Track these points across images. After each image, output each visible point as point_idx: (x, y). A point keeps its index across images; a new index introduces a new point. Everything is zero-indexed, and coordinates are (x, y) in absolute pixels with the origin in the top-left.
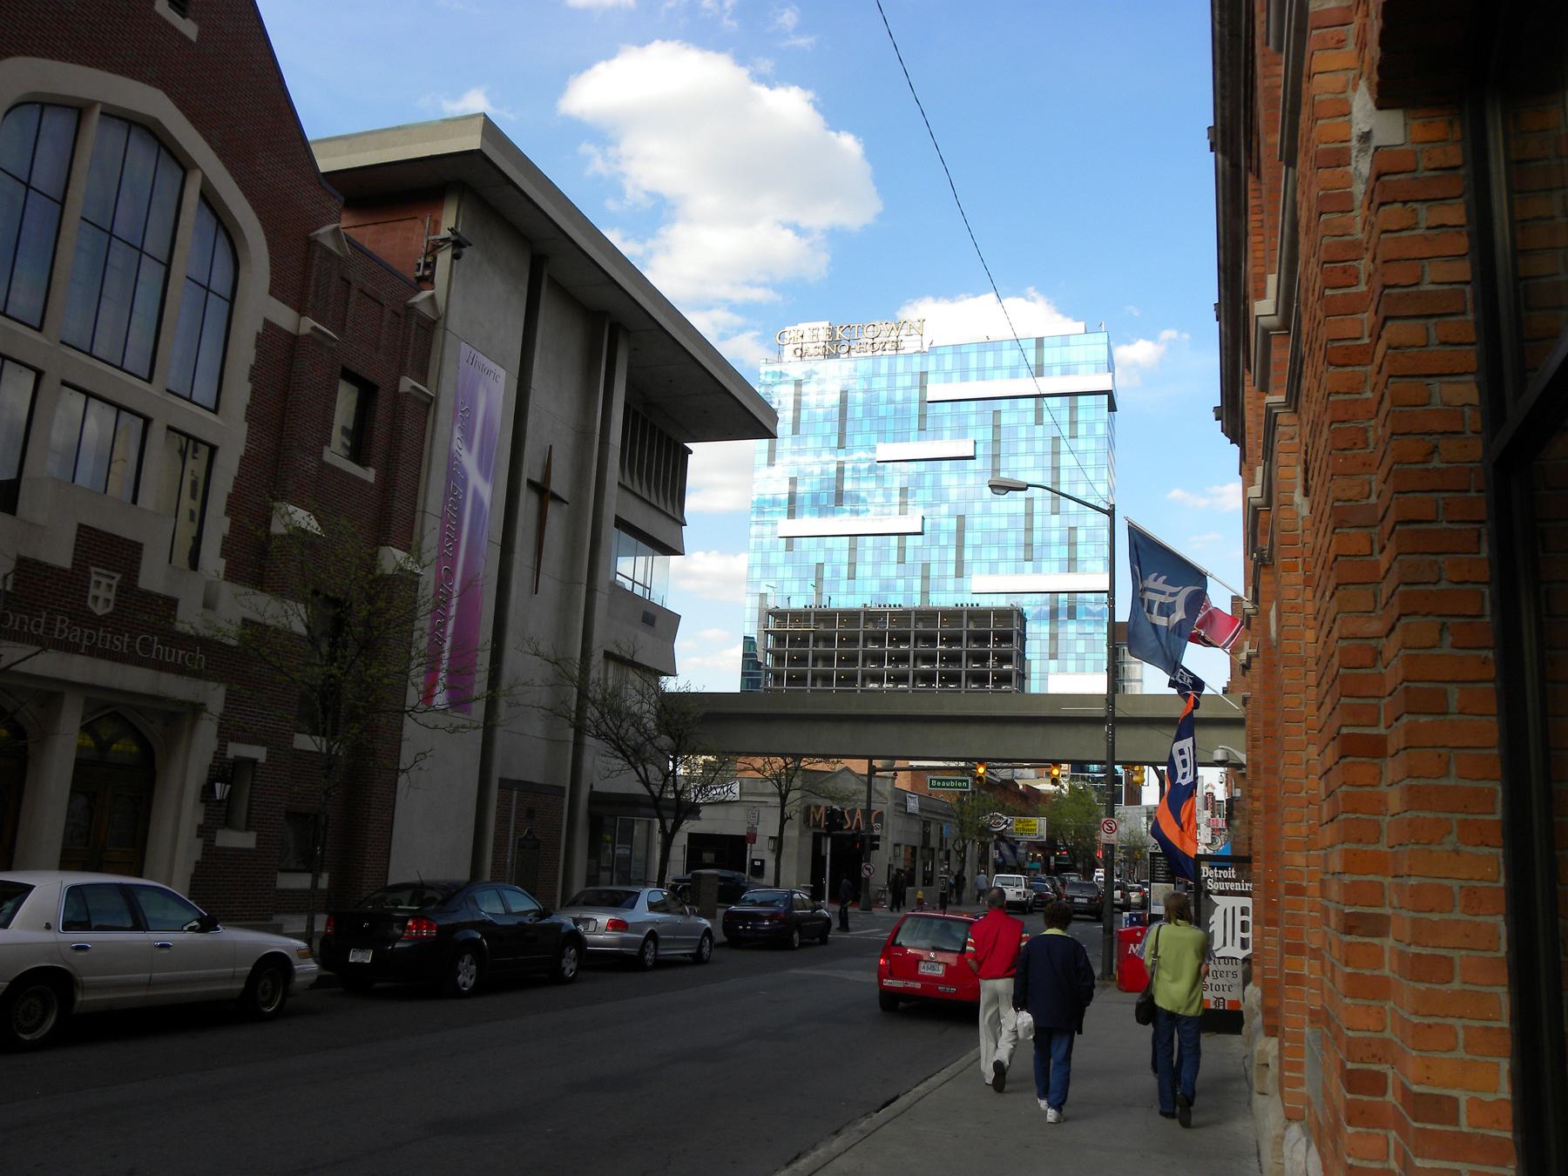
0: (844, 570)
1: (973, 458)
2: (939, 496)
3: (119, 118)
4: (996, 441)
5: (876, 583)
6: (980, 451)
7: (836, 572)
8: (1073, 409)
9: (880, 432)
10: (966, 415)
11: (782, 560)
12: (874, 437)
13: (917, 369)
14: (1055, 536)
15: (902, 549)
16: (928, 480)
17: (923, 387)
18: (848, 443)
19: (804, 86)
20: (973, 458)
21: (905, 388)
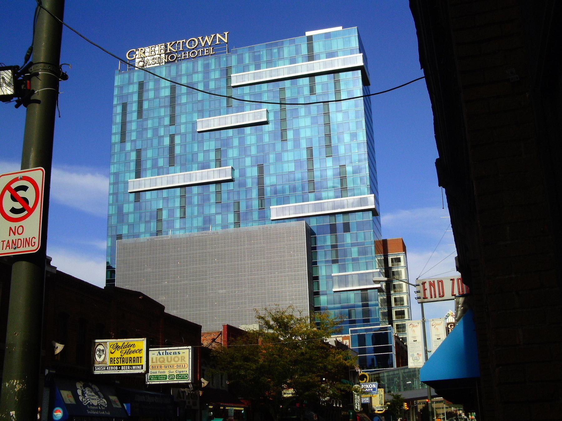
0: (178, 214)
1: (266, 123)
2: (244, 149)
3: (33, 44)
4: (328, 136)
5: (201, 219)
6: (271, 118)
7: (171, 212)
8: (337, 82)
9: (199, 111)
10: (229, 138)
11: (132, 209)
12: (195, 115)
13: (223, 66)
14: (330, 173)
15: (218, 193)
16: (236, 142)
17: (229, 79)
18: (177, 120)
19: (424, 366)
20: (266, 123)
21: (216, 80)
